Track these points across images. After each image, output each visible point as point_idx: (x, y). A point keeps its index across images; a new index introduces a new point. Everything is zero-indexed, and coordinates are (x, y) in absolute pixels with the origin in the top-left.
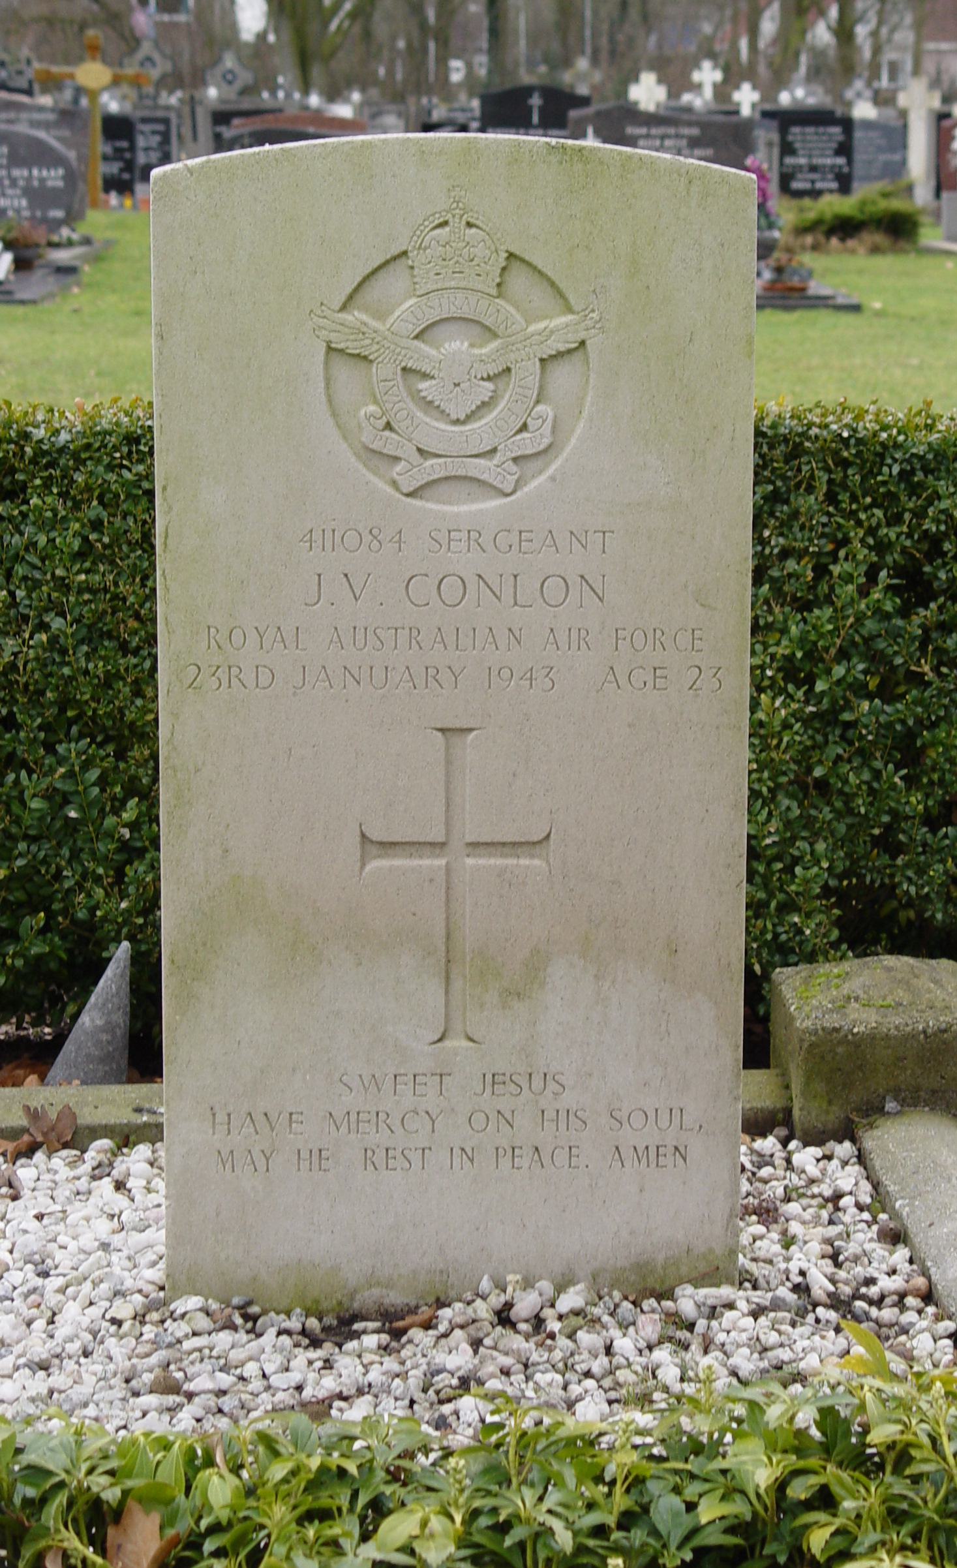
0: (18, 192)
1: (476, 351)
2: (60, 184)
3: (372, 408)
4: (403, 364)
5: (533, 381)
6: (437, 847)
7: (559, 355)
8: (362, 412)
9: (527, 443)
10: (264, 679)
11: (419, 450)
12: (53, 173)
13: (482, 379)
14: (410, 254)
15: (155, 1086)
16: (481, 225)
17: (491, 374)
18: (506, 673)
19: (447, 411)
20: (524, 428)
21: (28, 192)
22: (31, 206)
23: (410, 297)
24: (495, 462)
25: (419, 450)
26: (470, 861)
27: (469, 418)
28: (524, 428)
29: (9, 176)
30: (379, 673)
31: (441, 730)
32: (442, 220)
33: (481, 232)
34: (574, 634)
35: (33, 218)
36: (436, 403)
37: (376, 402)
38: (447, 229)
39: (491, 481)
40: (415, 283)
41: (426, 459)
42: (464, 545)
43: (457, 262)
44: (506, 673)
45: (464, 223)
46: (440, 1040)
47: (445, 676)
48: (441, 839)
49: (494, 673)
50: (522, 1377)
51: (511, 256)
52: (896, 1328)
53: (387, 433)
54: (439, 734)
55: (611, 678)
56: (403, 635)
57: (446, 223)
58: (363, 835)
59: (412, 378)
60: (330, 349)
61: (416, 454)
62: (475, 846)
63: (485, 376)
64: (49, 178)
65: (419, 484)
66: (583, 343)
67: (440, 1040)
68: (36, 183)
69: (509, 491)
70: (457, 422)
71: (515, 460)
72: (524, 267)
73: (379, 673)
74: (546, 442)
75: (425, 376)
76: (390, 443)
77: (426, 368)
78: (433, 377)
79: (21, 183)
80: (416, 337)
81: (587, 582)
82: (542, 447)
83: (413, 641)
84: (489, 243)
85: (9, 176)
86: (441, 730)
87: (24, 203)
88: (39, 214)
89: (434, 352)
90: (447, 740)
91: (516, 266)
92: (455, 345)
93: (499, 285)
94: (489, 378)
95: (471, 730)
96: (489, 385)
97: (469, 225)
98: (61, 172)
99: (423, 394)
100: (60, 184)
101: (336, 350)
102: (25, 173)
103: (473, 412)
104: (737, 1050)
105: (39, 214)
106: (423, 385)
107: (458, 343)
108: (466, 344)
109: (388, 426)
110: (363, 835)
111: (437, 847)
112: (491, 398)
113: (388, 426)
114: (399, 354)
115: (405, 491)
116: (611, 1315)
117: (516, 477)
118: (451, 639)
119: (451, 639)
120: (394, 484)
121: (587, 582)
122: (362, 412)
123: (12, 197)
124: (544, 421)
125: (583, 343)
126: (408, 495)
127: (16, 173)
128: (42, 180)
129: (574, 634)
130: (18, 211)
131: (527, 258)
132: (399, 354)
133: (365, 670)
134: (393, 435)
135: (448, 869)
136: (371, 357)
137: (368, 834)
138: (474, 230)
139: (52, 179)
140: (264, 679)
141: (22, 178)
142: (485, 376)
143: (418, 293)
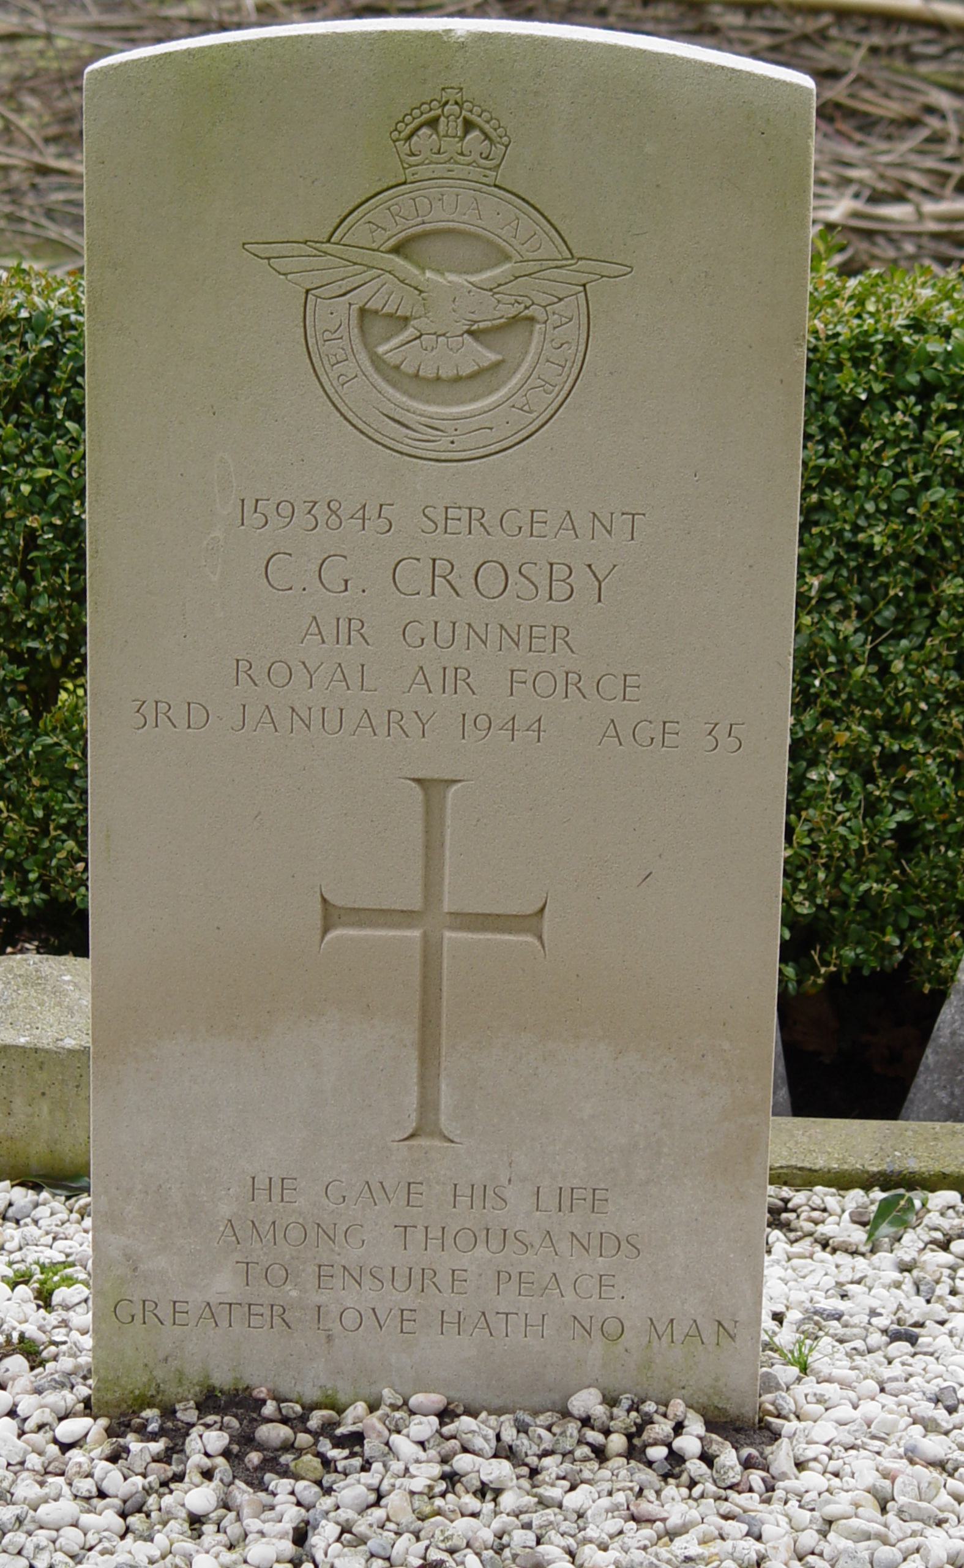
10: (198, 716)
18: (483, 722)
26: (448, 934)
30: (332, 716)
31: (418, 781)
34: (450, 673)
42: (463, 526)
44: (483, 722)
46: (412, 1136)
47: (412, 725)
48: (417, 904)
49: (469, 722)
52: (846, 296)
54: (416, 788)
55: (365, 722)
58: (324, 900)
73: (332, 716)
81: (506, 631)
83: (242, 675)
86: (418, 781)
104: (954, 1133)
110: (324, 900)
111: (406, 917)
116: (921, 1500)
121: (506, 631)
129: (450, 673)
133: (316, 714)
135: (425, 935)
140: (198, 716)
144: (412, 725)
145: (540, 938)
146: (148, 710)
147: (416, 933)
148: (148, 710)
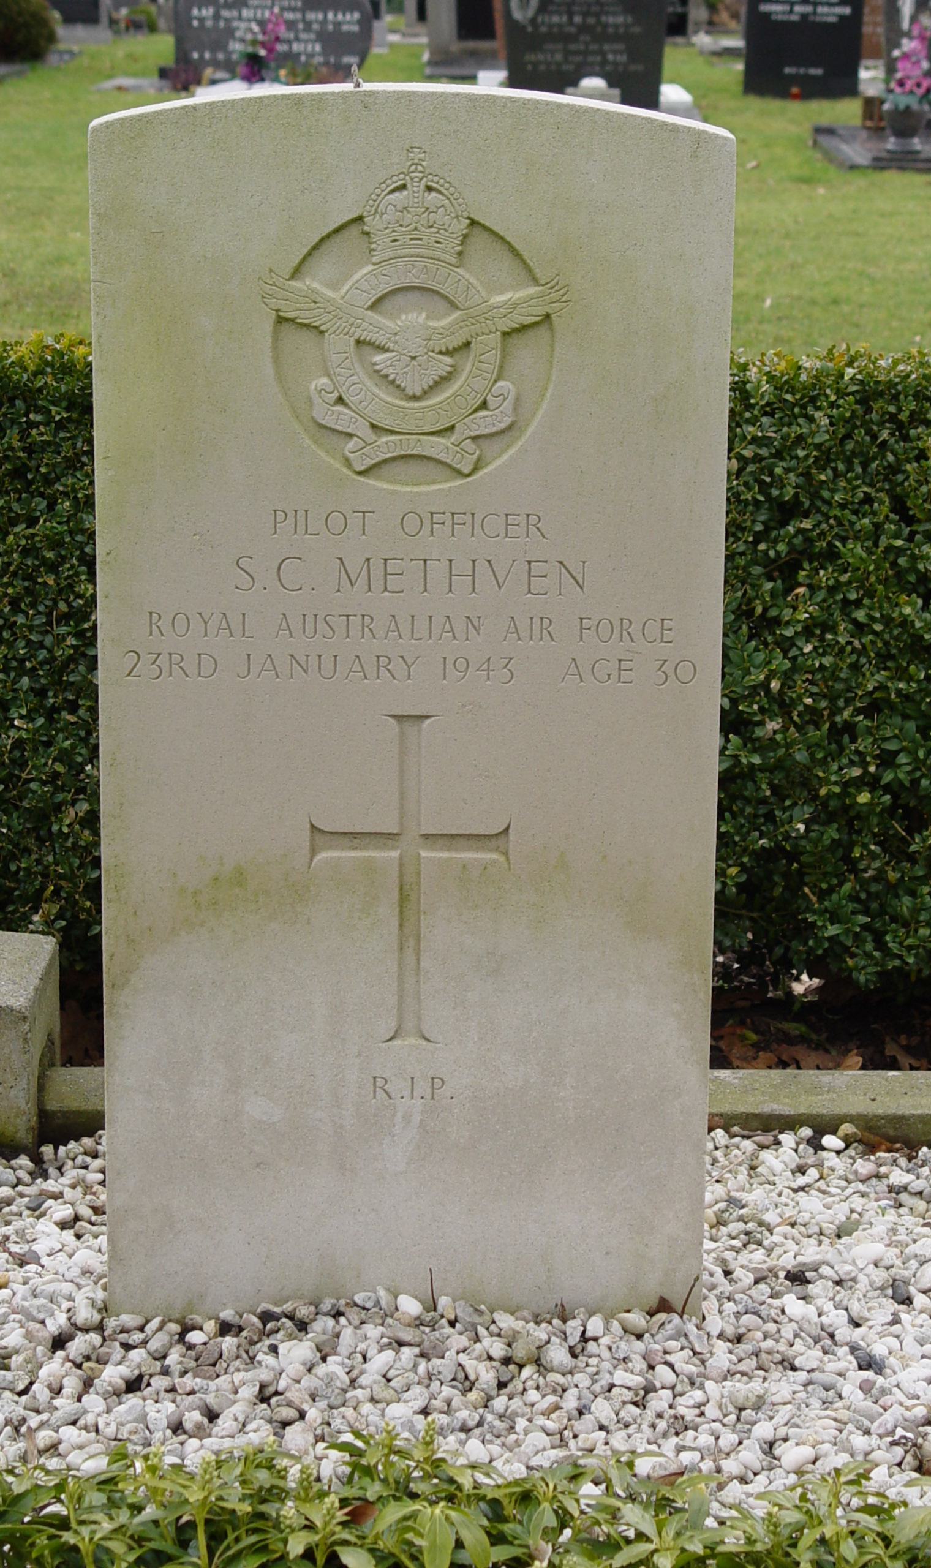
0: (312, 36)
1: (431, 323)
2: (355, 28)
3: (325, 380)
4: (356, 336)
5: (493, 357)
6: (388, 838)
7: (524, 328)
8: (313, 387)
9: (484, 423)
11: (373, 426)
12: (348, 17)
13: (441, 353)
14: (366, 220)
15: (97, 1069)
16: (442, 189)
17: (451, 348)
19: (403, 385)
20: (484, 405)
21: (322, 37)
22: (325, 52)
23: (367, 264)
24: (453, 439)
25: (373, 426)
26: (423, 854)
27: (426, 393)
28: (484, 405)
29: (304, 20)
30: (327, 664)
31: (399, 718)
32: (399, 183)
33: (441, 197)
34: (537, 621)
35: (326, 64)
36: (391, 377)
37: (329, 375)
38: (405, 193)
39: (448, 461)
40: (371, 250)
41: (379, 437)
43: (416, 229)
45: (422, 187)
46: (391, 1039)
47: (398, 666)
50: (194, 1443)
51: (473, 223)
53: (339, 408)
56: (355, 621)
57: (404, 187)
58: (312, 826)
59: (367, 350)
60: (281, 320)
61: (369, 431)
62: (428, 838)
63: (444, 349)
64: (345, 22)
65: (373, 462)
66: (548, 316)
67: (391, 1039)
68: (330, 27)
69: (466, 471)
70: (415, 398)
71: (474, 439)
72: (486, 234)
74: (508, 421)
75: (383, 349)
76: (340, 417)
77: (380, 339)
78: (388, 350)
79: (316, 26)
80: (373, 307)
82: (503, 426)
84: (450, 208)
85: (304, 20)
87: (318, 48)
88: (332, 60)
89: (389, 324)
90: (402, 735)
91: (477, 231)
92: (412, 316)
93: (460, 253)
94: (447, 353)
95: (427, 717)
96: (448, 360)
97: (429, 189)
98: (356, 16)
99: (378, 368)
100: (355, 28)
101: (287, 320)
102: (320, 16)
103: (431, 387)
105: (332, 60)
106: (378, 358)
107: (415, 315)
108: (424, 315)
109: (340, 400)
110: (312, 826)
111: (388, 838)
112: (450, 373)
113: (340, 400)
114: (352, 325)
115: (358, 469)
117: (475, 457)
118: (405, 626)
119: (405, 626)
120: (348, 463)
122: (313, 387)
123: (306, 41)
124: (504, 400)
125: (548, 316)
126: (360, 473)
127: (311, 16)
128: (338, 24)
130: (311, 56)
131: (487, 224)
132: (352, 325)
133: (313, 661)
134: (346, 411)
135: (401, 855)
136: (322, 328)
137: (316, 824)
138: (434, 194)
139: (349, 23)
141: (317, 21)
142: (444, 349)
143: (374, 259)
144: (398, 666)
145: (506, 854)
146: (163, 660)
147: (395, 854)
148: (163, 660)
